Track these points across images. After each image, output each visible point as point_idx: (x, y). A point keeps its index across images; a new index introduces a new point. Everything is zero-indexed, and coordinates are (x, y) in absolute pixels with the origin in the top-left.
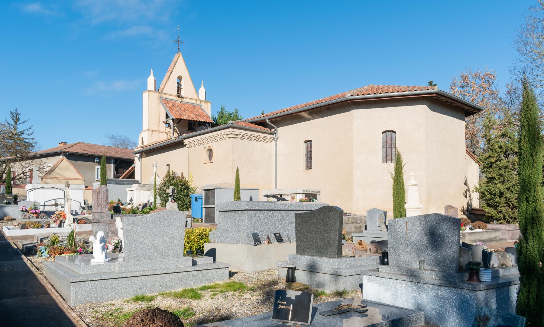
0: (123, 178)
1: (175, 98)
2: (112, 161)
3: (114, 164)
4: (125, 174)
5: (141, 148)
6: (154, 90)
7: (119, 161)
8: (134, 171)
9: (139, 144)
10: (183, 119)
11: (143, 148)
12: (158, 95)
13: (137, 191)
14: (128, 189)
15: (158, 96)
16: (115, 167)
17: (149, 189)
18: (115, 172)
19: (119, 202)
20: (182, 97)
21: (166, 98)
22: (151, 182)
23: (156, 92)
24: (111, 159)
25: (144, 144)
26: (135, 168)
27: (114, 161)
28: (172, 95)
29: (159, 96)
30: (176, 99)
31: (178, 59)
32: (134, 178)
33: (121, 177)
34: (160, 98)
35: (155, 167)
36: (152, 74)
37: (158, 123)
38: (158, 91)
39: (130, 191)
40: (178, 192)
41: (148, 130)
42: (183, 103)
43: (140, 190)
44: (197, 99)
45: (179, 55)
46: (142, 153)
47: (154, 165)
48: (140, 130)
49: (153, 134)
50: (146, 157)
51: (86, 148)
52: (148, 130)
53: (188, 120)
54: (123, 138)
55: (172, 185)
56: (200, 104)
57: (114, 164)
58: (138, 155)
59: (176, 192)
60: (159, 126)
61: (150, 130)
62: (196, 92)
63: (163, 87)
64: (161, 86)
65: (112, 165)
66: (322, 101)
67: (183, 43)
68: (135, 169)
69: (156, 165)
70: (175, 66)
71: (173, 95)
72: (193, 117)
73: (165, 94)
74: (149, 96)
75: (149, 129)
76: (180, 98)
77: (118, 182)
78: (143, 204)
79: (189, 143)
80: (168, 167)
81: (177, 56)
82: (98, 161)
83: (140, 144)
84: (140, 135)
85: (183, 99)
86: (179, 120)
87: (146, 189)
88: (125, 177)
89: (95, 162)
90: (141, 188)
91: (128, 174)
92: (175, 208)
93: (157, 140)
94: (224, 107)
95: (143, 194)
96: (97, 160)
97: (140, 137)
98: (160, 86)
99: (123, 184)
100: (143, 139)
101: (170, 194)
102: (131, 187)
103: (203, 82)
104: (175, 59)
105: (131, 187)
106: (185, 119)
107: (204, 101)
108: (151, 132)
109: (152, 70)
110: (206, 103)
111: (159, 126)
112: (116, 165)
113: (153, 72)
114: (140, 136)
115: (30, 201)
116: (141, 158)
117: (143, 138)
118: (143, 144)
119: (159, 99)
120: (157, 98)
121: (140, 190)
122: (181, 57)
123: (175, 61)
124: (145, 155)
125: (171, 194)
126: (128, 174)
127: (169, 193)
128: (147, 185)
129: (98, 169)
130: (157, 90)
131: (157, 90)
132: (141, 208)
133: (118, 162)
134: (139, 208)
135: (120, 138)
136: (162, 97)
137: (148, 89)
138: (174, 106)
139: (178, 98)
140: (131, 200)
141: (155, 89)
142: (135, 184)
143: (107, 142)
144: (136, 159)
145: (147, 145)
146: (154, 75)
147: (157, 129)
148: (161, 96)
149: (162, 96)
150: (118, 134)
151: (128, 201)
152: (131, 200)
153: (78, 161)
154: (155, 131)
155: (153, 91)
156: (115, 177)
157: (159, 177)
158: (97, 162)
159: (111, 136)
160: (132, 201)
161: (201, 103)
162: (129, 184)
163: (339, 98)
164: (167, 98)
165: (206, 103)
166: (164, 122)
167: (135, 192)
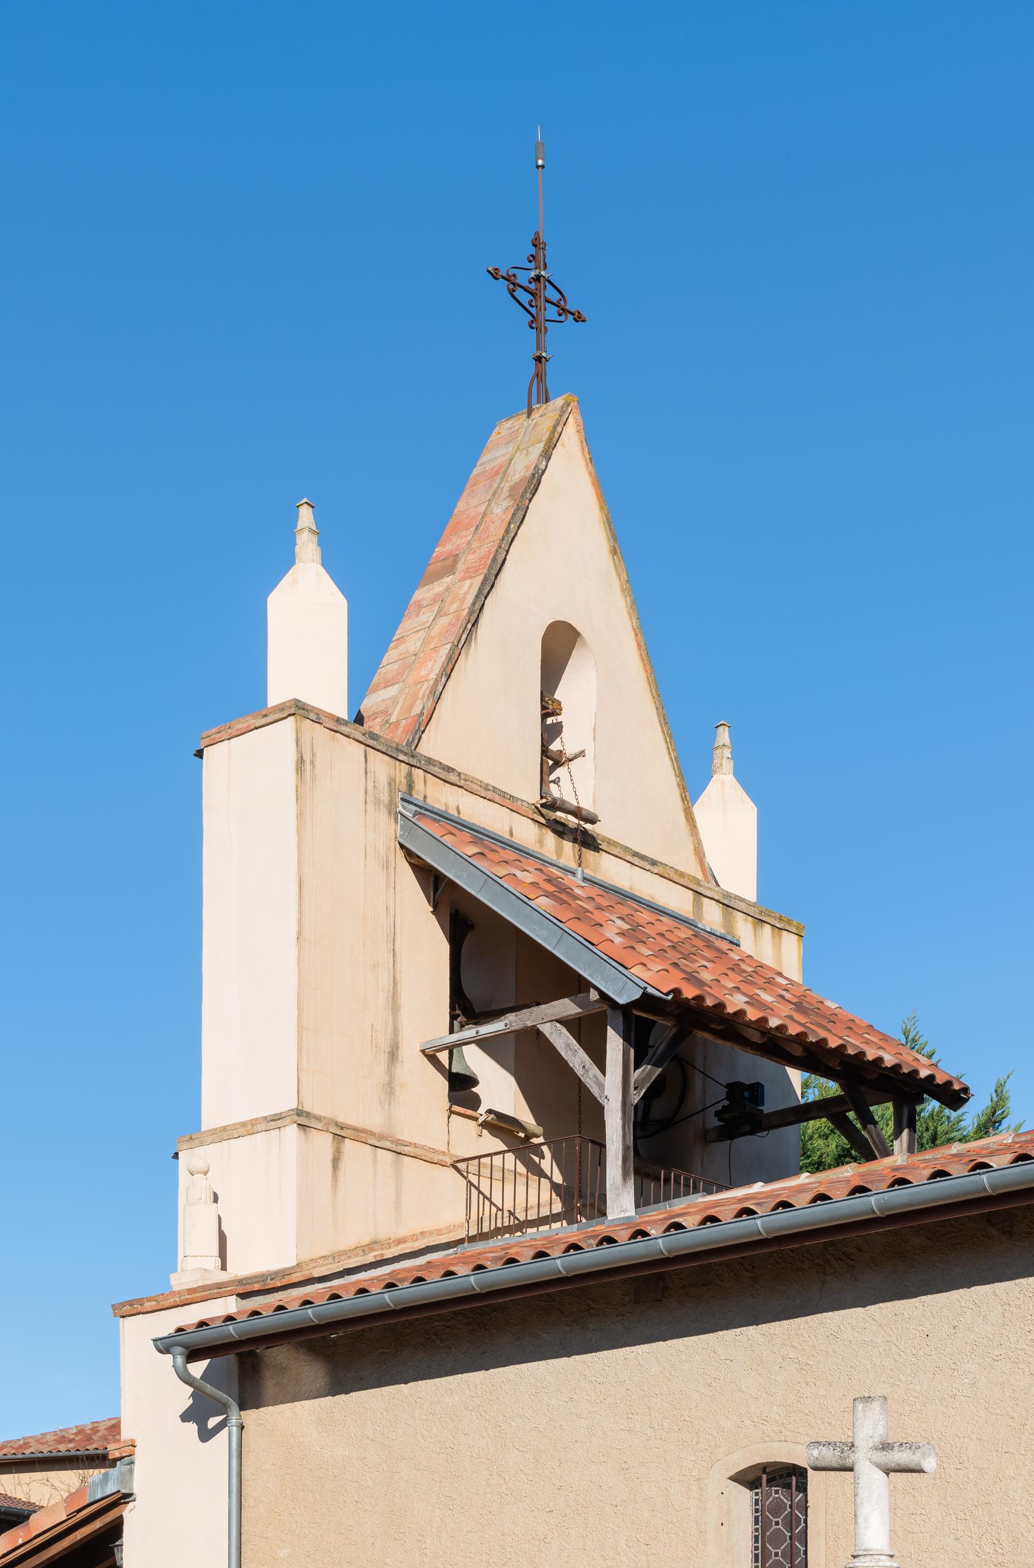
5: (230, 1305)
8: (115, 1530)
11: (254, 1303)
15: (383, 780)
20: (587, 841)
26: (131, 1516)
28: (503, 794)
29: (391, 782)
30: (541, 842)
31: (547, 455)
37: (384, 1059)
45: (559, 423)
50: (338, 1386)
60: (389, 1089)
61: (318, 1119)
66: (452, 1269)
70: (519, 516)
71: (507, 801)
73: (446, 774)
74: (300, 762)
75: (307, 1108)
76: (568, 846)
85: (589, 855)
93: (385, 1232)
108: (323, 1142)
109: (306, 517)
111: (389, 1089)
113: (322, 534)
115: (418, 750)
119: (396, 815)
120: (377, 802)
122: (571, 437)
139: (550, 837)
145: (295, 1278)
146: (327, 563)
147: (370, 1119)
148: (410, 786)
149: (419, 786)
154: (361, 1135)
155: (338, 720)
161: (728, 922)
163: (419, 1279)
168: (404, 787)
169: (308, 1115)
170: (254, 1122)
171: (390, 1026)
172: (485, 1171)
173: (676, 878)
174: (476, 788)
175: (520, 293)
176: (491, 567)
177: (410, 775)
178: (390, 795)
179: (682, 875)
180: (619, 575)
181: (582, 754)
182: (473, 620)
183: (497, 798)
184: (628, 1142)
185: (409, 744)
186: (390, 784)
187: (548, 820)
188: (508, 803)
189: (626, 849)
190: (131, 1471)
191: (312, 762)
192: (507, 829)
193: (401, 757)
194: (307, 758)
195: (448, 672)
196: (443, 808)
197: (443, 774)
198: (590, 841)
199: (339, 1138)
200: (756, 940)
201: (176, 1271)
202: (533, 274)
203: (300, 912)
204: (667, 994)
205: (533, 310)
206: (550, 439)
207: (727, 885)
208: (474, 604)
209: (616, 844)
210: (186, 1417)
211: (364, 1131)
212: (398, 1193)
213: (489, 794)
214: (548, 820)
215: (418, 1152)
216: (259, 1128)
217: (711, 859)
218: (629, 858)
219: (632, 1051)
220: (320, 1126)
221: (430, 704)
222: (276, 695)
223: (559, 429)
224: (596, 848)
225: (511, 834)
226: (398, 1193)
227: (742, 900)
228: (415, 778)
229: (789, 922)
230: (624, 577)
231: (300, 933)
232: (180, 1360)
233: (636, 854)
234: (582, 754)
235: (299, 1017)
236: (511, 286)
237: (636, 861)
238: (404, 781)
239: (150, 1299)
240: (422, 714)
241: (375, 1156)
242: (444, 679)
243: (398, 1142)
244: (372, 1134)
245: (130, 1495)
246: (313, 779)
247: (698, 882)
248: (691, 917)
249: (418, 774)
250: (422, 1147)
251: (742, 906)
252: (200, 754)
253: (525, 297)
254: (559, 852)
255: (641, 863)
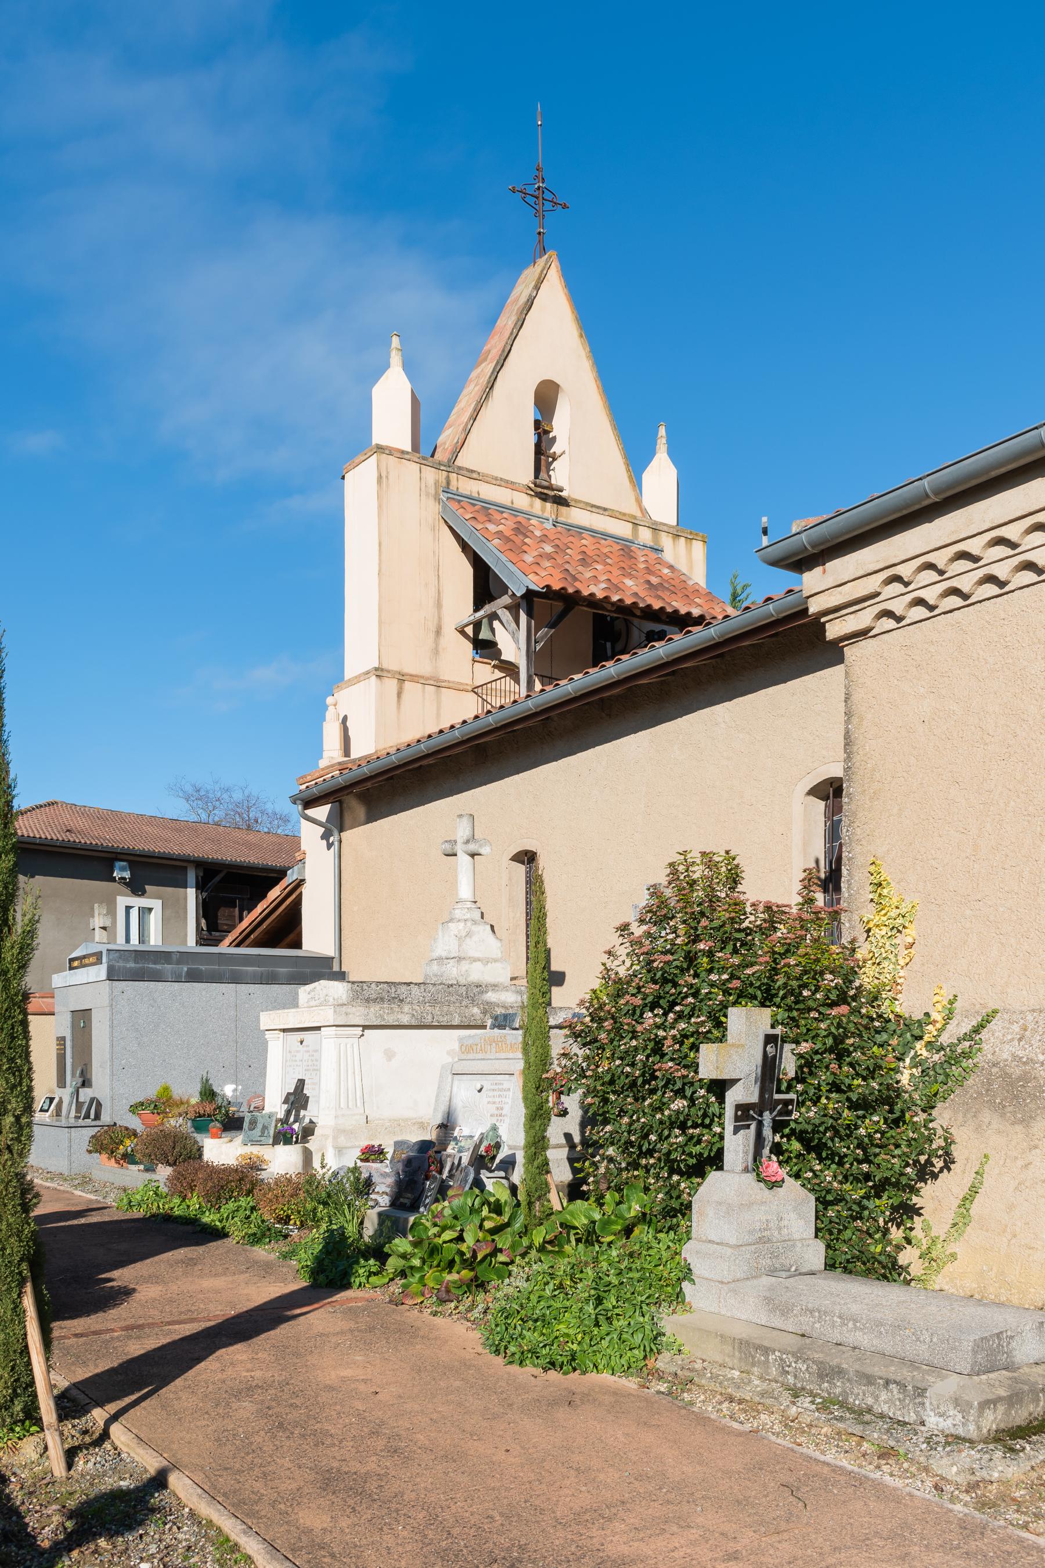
0: (238, 945)
1: (522, 501)
2: (191, 876)
3: (200, 887)
4: (245, 923)
6: (409, 448)
7: (221, 875)
8: (298, 903)
9: (325, 754)
10: (585, 599)
12: (431, 475)
13: (337, 1037)
14: (268, 1020)
15: (431, 482)
16: (204, 900)
17: (428, 1020)
18: (203, 922)
19: (209, 1108)
20: (561, 502)
21: (475, 495)
22: (435, 967)
23: (422, 462)
24: (185, 868)
25: (355, 754)
26: (306, 891)
27: (197, 878)
28: (507, 481)
29: (437, 483)
30: (532, 506)
31: (537, 288)
32: (297, 944)
33: (227, 941)
34: (443, 497)
35: (463, 859)
36: (396, 359)
37: (432, 635)
38: (433, 456)
39: (284, 1030)
40: (807, 1066)
41: (379, 672)
42: (569, 530)
43: (365, 1027)
44: (639, 514)
46: (340, 802)
47: (459, 849)
48: (336, 679)
49: (405, 696)
50: (371, 818)
51: (80, 823)
52: (379, 672)
53: (613, 604)
54: (238, 796)
55: (767, 999)
56: (650, 543)
57: (197, 888)
58: (322, 812)
59: (789, 1066)
60: (436, 651)
61: (388, 671)
62: (630, 477)
63: (459, 436)
64: (447, 438)
65: (191, 893)
67: (565, 207)
68: (301, 893)
69: (472, 847)
70: (520, 324)
71: (511, 485)
72: (635, 589)
73: (471, 474)
74: (380, 477)
75: (385, 666)
76: (548, 505)
77: (203, 968)
78: (398, 1144)
79: (873, 584)
80: (521, 869)
81: (530, 274)
82: (127, 875)
83: (331, 753)
84: (330, 700)
86: (559, 606)
87: (405, 1020)
88: (248, 941)
89: (113, 880)
90: (373, 1013)
91: (264, 926)
92: (789, 1243)
94: (745, 587)
95: (390, 1055)
96: (122, 869)
97: (330, 714)
98: (441, 439)
99: (236, 979)
100: (348, 724)
101: (734, 1096)
102: (294, 1003)
103: (662, 431)
104: (522, 290)
105: (294, 1003)
106: (600, 595)
107: (673, 527)
108: (392, 684)
110: (682, 539)
111: (436, 651)
112: (205, 894)
114: (331, 709)
116: (341, 830)
117: (345, 718)
118: (347, 752)
119: (438, 500)
120: (427, 494)
121: (365, 1027)
122: (554, 281)
123: (523, 300)
124: (361, 811)
125: (754, 1098)
126: (264, 926)
127: (719, 1087)
128: (415, 989)
129: (128, 909)
130: (426, 451)
131: (426, 451)
132: (390, 1180)
133: (218, 878)
134: (369, 1183)
135: (225, 796)
136: (453, 488)
137: (377, 439)
138: (527, 537)
139: (538, 502)
140: (297, 1099)
141: (416, 447)
142: (323, 983)
143: (176, 809)
144: (310, 836)
147: (424, 669)
148: (448, 483)
150: (217, 782)
151: (275, 1105)
152: (297, 1099)
153: (37, 877)
154: (415, 678)
155: (403, 452)
156: (201, 941)
157: (492, 927)
158: (125, 879)
159: (189, 789)
160: (305, 1107)
161: (656, 538)
162: (270, 980)
164: (483, 496)
165: (682, 539)
166: (462, 632)
167: (328, 1040)
168: (444, 484)
169: (382, 670)
170: (359, 676)
171: (436, 617)
172: (484, 692)
173: (620, 517)
174: (489, 479)
175: (529, 199)
176: (501, 355)
177: (448, 477)
178: (436, 489)
179: (624, 514)
180: (585, 349)
181: (564, 452)
182: (490, 386)
183: (503, 483)
184: (530, 673)
185: (449, 461)
186: (435, 484)
187: (536, 493)
188: (510, 486)
189: (587, 504)
190: (304, 867)
191: (387, 477)
192: (510, 500)
193: (442, 468)
194: (384, 475)
195: (474, 418)
196: (469, 493)
197: (468, 474)
198: (563, 502)
199: (401, 681)
200: (674, 548)
201: (322, 758)
202: (536, 186)
203: (380, 560)
204: (543, 588)
205: (537, 207)
206: (539, 278)
207: (656, 517)
208: (490, 377)
209: (580, 501)
210: (322, 838)
211: (416, 676)
212: (439, 708)
213: (498, 482)
214: (536, 493)
215: (451, 685)
216: (362, 678)
217: (646, 502)
218: (589, 508)
219: (533, 622)
220: (389, 675)
221: (463, 436)
222: (377, 439)
223: (545, 272)
224: (568, 505)
225: (512, 503)
226: (439, 708)
227: (665, 525)
228: (451, 478)
229: (696, 535)
230: (588, 349)
231: (380, 571)
232: (300, 807)
233: (593, 506)
234: (564, 452)
235: (380, 616)
236: (523, 195)
237: (594, 509)
238: (444, 481)
239: (309, 775)
240: (457, 442)
241: (424, 691)
242: (471, 422)
243: (438, 680)
244: (422, 677)
245: (304, 880)
246: (388, 486)
247: (635, 517)
248: (630, 538)
249: (453, 476)
250: (453, 682)
251: (665, 528)
252: (343, 478)
253: (531, 200)
254: (543, 510)
255: (598, 510)
